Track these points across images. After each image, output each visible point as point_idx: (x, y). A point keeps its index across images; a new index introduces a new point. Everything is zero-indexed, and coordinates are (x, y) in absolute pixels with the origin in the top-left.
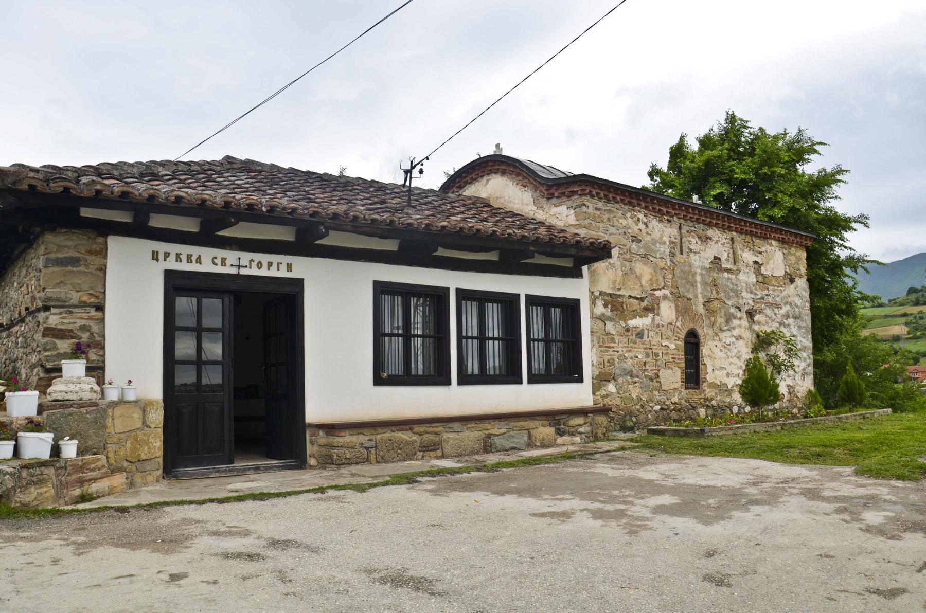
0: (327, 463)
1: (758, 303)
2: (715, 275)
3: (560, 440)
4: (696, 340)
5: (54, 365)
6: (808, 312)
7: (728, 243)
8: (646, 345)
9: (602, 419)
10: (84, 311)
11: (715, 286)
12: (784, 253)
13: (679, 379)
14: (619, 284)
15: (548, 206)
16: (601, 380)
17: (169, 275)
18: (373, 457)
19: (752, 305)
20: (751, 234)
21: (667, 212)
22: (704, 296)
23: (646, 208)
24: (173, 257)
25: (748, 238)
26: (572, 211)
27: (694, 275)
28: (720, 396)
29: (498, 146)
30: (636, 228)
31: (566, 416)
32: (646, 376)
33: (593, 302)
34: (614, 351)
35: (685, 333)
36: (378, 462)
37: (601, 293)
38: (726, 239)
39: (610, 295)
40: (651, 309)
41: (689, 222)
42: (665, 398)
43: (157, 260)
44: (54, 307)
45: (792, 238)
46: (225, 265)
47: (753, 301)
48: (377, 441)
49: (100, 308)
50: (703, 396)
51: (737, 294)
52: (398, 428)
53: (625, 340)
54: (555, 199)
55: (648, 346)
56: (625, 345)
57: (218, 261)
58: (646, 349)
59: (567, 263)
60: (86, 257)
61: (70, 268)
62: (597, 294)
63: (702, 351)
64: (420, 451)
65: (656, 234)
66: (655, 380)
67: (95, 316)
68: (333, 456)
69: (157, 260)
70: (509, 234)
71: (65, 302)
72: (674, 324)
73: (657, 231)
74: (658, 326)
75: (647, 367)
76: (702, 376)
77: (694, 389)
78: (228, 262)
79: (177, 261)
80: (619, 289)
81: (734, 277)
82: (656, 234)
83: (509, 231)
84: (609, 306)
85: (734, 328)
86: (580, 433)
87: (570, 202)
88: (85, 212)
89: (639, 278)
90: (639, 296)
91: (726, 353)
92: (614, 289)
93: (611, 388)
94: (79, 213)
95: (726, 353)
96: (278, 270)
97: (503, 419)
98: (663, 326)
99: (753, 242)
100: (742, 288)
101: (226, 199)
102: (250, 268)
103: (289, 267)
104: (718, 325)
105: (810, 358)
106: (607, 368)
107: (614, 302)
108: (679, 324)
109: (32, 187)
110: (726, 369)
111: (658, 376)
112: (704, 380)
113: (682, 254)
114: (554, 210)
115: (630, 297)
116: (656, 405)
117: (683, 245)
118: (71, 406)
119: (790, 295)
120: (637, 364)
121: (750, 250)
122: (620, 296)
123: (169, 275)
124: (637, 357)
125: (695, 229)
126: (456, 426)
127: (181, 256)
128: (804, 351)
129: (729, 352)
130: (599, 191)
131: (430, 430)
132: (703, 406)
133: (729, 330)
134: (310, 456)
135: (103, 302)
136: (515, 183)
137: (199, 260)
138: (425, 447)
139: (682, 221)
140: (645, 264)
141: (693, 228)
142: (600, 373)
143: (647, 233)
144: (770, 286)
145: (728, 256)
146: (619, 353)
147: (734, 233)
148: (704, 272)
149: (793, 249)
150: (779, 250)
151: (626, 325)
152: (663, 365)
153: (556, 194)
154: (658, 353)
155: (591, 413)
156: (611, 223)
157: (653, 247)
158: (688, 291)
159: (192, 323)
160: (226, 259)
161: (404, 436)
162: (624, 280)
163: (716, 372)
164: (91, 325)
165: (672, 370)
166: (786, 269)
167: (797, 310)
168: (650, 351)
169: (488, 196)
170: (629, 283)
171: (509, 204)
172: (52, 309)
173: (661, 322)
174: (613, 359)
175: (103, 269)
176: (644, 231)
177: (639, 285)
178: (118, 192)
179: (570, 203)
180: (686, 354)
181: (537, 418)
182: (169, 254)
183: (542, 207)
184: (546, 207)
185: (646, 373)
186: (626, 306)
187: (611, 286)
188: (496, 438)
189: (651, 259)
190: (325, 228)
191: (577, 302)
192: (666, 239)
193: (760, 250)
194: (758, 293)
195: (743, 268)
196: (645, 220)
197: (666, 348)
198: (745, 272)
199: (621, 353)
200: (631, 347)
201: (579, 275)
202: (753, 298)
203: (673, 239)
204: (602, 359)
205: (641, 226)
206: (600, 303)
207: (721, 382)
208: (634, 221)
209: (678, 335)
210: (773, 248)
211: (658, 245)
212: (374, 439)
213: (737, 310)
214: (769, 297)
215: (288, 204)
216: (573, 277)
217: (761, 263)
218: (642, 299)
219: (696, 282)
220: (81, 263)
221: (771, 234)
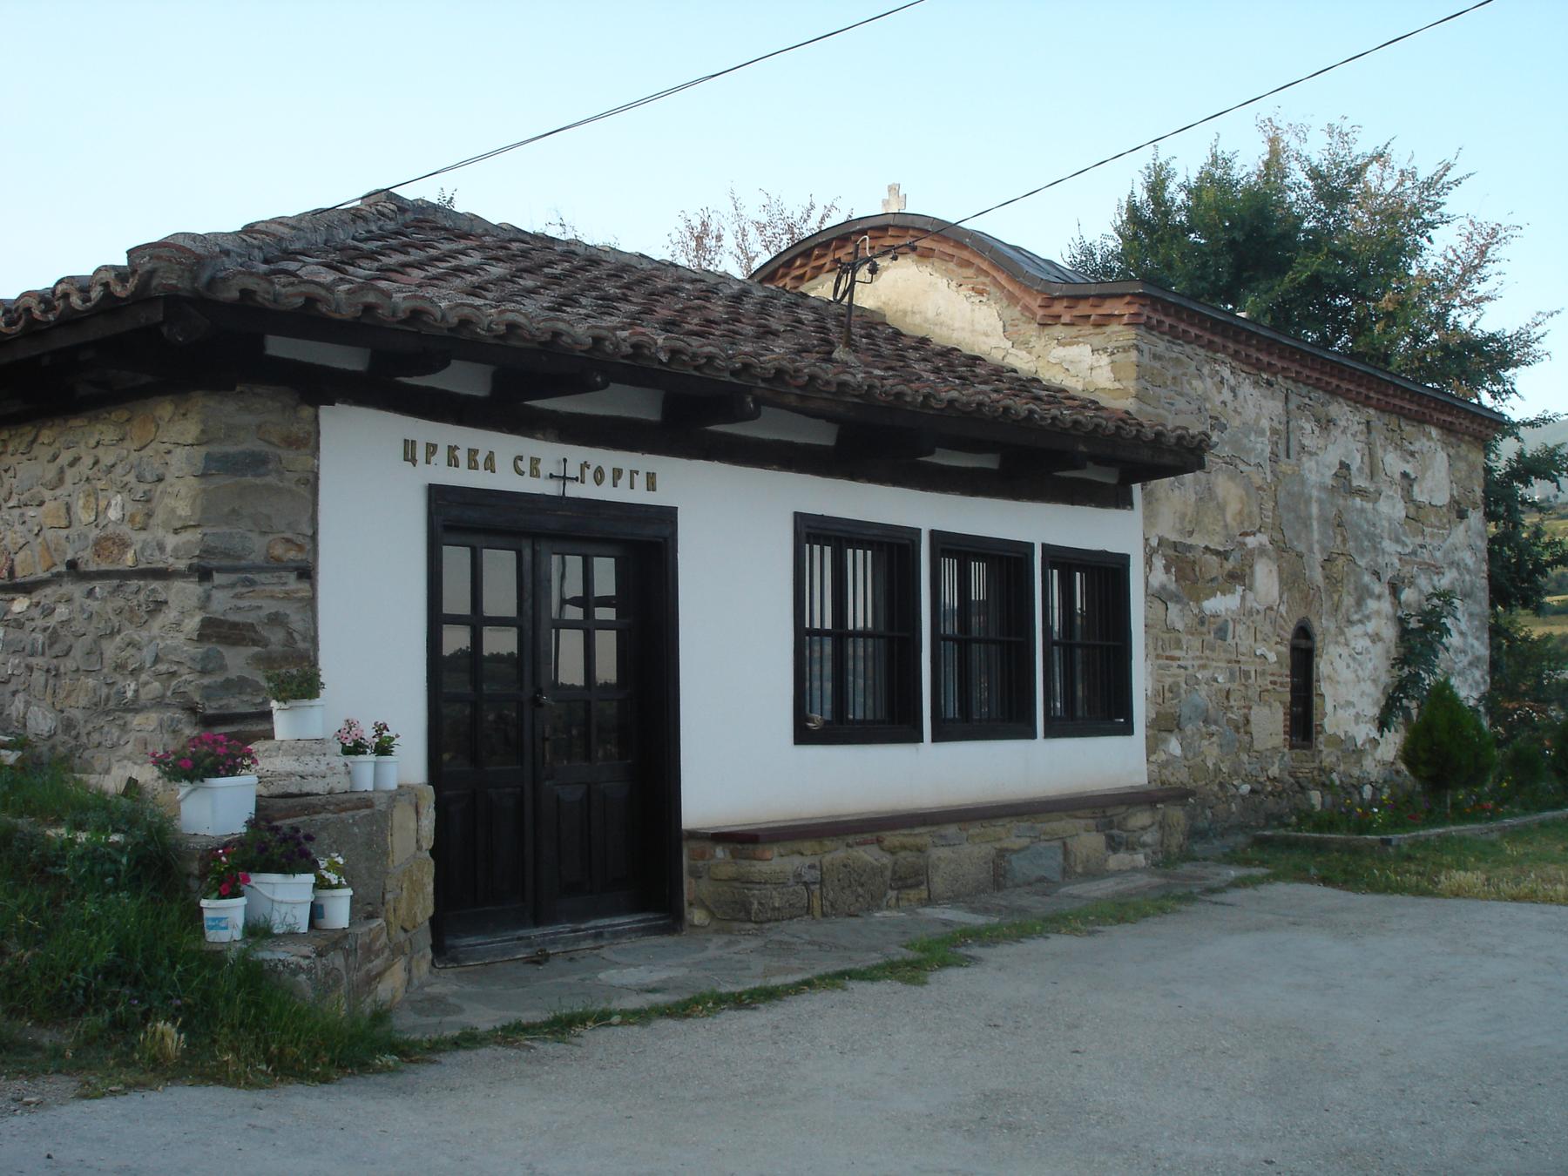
0: (735, 920)
1: (1407, 562)
2: (1341, 502)
3: (1116, 861)
4: (1309, 644)
5: (221, 707)
6: (1485, 582)
7: (1362, 432)
8: (1231, 653)
9: (1177, 814)
10: (275, 580)
11: (1338, 526)
12: (1449, 455)
13: (1281, 729)
14: (1190, 522)
15: (1043, 342)
16: (1164, 725)
17: (438, 496)
18: (816, 903)
19: (1399, 567)
20: (1401, 413)
21: (1269, 364)
22: (1324, 549)
23: (1235, 355)
24: (441, 456)
25: (1394, 419)
26: (1105, 360)
27: (1308, 501)
28: (1345, 763)
29: (894, 189)
30: (1217, 399)
31: (1122, 809)
32: (1229, 720)
33: (1149, 562)
34: (1180, 667)
35: (1292, 627)
36: (824, 915)
37: (1161, 542)
38: (1359, 423)
39: (1175, 545)
40: (1239, 577)
41: (1301, 385)
42: (1258, 767)
43: (414, 462)
44: (220, 570)
45: (1466, 423)
46: (538, 476)
47: (1400, 560)
48: (825, 869)
49: (307, 573)
50: (1315, 765)
51: (1375, 540)
52: (859, 838)
53: (1197, 643)
54: (1059, 328)
55: (1234, 657)
56: (1198, 654)
57: (525, 466)
58: (1229, 662)
59: (1108, 477)
60: (279, 452)
61: (249, 479)
62: (1154, 542)
63: (1318, 668)
64: (892, 888)
65: (1250, 412)
66: (1242, 730)
67: (297, 591)
68: (751, 904)
69: (414, 462)
70: (1054, 418)
71: (239, 558)
72: (1275, 608)
73: (1251, 406)
74: (1251, 613)
75: (1232, 703)
76: (1316, 721)
77: (1304, 748)
78: (544, 468)
79: (450, 465)
80: (1191, 533)
81: (1368, 506)
82: (1250, 412)
83: (1055, 412)
84: (1173, 570)
85: (1368, 618)
86: (1144, 845)
87: (1100, 337)
88: (278, 347)
89: (1221, 508)
90: (1221, 549)
91: (1356, 671)
92: (1181, 532)
93: (1174, 746)
94: (263, 347)
95: (1356, 671)
96: (632, 488)
97: (1026, 817)
98: (1258, 612)
99: (1402, 431)
100: (1382, 531)
101: (597, 332)
102: (583, 482)
103: (651, 485)
104: (1344, 611)
105: (1485, 681)
106: (1167, 704)
107: (1179, 558)
108: (1283, 609)
109: (246, 293)
110: (1354, 707)
111: (1248, 721)
112: (1319, 728)
113: (1288, 456)
114: (1059, 352)
115: (1207, 548)
116: (1244, 782)
117: (1292, 437)
118: (324, 808)
119: (1458, 545)
120: (1216, 695)
121: (1396, 449)
122: (1190, 548)
123: (438, 496)
124: (1216, 680)
125: (1311, 403)
126: (951, 830)
127: (457, 453)
128: (1477, 667)
129: (1359, 669)
130: (1163, 318)
131: (910, 841)
132: (1317, 785)
133: (1361, 621)
134: (691, 904)
135: (310, 560)
136: (953, 284)
137: (490, 465)
138: (900, 878)
139: (1290, 384)
140: (1232, 478)
141: (1307, 401)
142: (1157, 713)
143: (1235, 410)
144: (1427, 526)
145: (1362, 462)
146: (1188, 672)
147: (1372, 411)
148: (1324, 496)
149: (1463, 446)
150: (1442, 449)
151: (1201, 611)
152: (1257, 698)
153: (1066, 318)
154: (1249, 672)
155: (1162, 801)
156: (1178, 389)
157: (1245, 441)
158: (1298, 538)
159: (465, 609)
160: (538, 460)
161: (868, 855)
162: (1198, 513)
163: (1340, 712)
164: (288, 612)
165: (1270, 706)
166: (1452, 489)
167: (1467, 578)
168: (1236, 666)
169: (880, 304)
170: (1206, 520)
171: (937, 329)
172: (216, 575)
173: (1255, 604)
174: (1177, 684)
175: (311, 482)
176: (1230, 406)
177: (1222, 523)
178: (404, 311)
179: (1098, 341)
180: (1293, 675)
181: (1079, 813)
182: (435, 446)
183: (1026, 344)
184: (1037, 344)
185: (1230, 715)
186: (1201, 570)
187: (1178, 526)
188: (1014, 857)
189: (1242, 467)
190: (755, 401)
191: (1123, 560)
192: (1265, 423)
193: (1412, 448)
194: (1408, 541)
195: (1387, 491)
196: (1232, 382)
197: (1263, 660)
198: (1388, 497)
199: (1190, 671)
200: (1207, 658)
201: (1124, 501)
202: (1400, 553)
203: (1276, 424)
204: (1161, 684)
205: (1226, 395)
206: (1159, 562)
207: (1346, 732)
208: (1214, 384)
209: (1282, 632)
210: (1432, 444)
211: (1252, 438)
212: (818, 864)
213: (1375, 578)
214: (1424, 551)
215: (702, 346)
216: (1117, 506)
217: (1413, 477)
218: (1224, 555)
219: (1310, 517)
220: (270, 467)
221: (1433, 413)
